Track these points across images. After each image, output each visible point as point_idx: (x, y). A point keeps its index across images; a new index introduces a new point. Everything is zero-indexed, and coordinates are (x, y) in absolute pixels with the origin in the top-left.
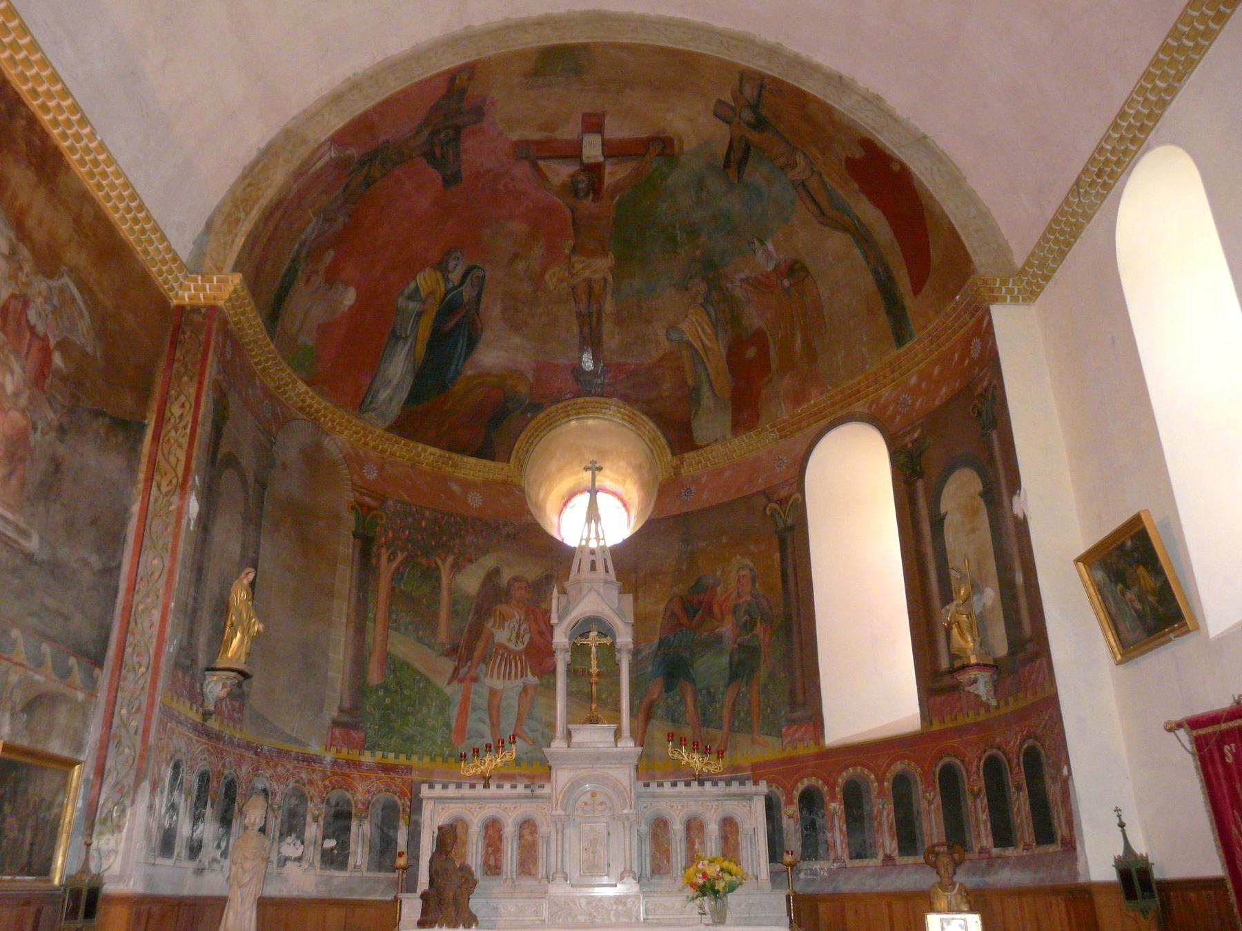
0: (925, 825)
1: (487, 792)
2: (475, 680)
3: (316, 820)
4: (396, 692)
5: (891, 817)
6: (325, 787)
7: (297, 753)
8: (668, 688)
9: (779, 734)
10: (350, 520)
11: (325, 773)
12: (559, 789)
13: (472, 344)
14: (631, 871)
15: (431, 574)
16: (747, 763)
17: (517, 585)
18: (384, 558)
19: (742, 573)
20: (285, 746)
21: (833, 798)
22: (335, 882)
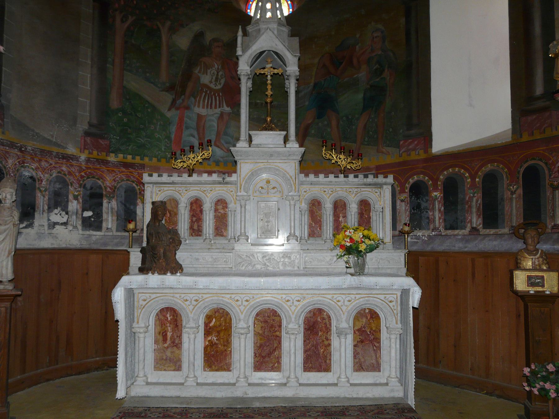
0: (507, 208)
1: (191, 179)
3: (76, 198)
5: (479, 202)
6: (82, 177)
7: (57, 153)
8: (320, 116)
9: (398, 146)
11: (80, 167)
12: (242, 176)
14: (294, 235)
19: (375, 35)
20: (47, 148)
21: (436, 189)
22: (94, 238)
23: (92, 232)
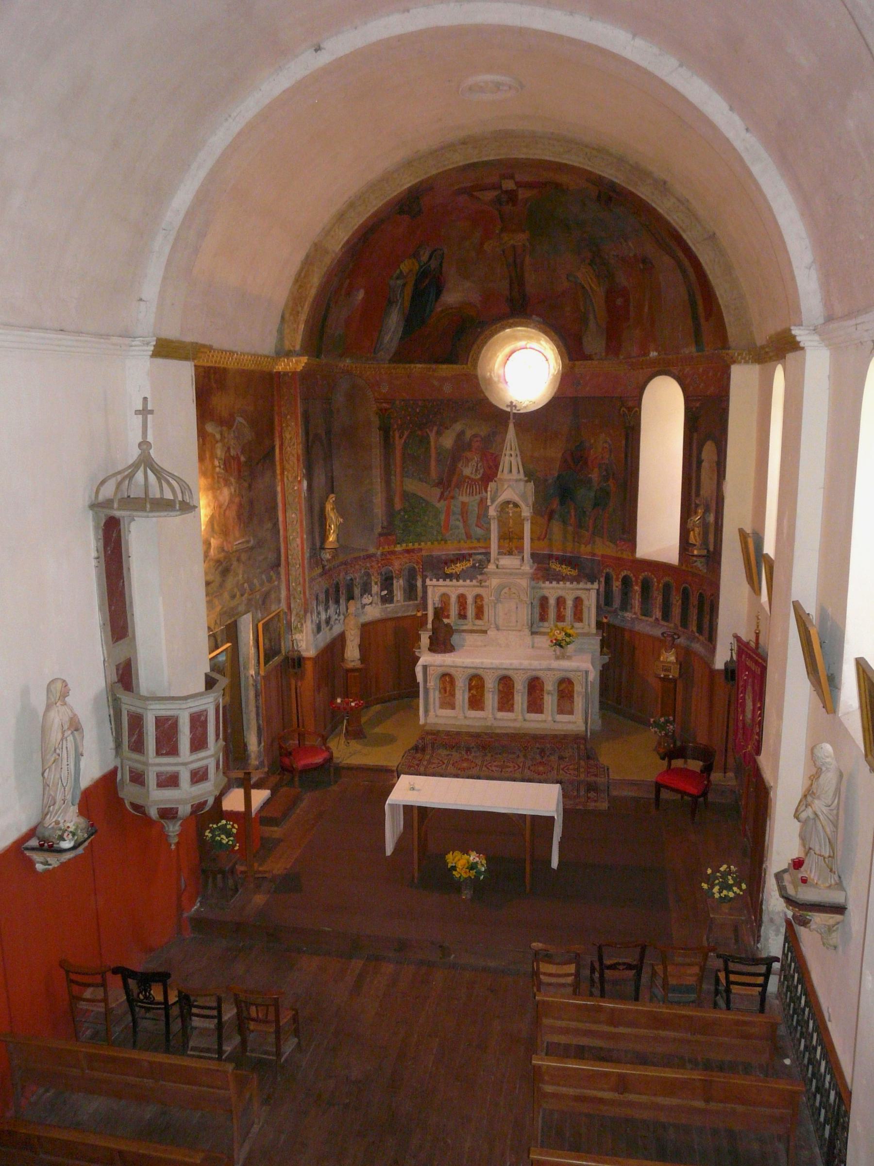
2: (453, 498)
3: (376, 583)
4: (410, 511)
6: (379, 567)
10: (376, 421)
13: (439, 293)
15: (424, 441)
16: (600, 553)
17: (475, 439)
18: (397, 435)
21: (637, 584)
22: (389, 610)
23: (387, 605)
